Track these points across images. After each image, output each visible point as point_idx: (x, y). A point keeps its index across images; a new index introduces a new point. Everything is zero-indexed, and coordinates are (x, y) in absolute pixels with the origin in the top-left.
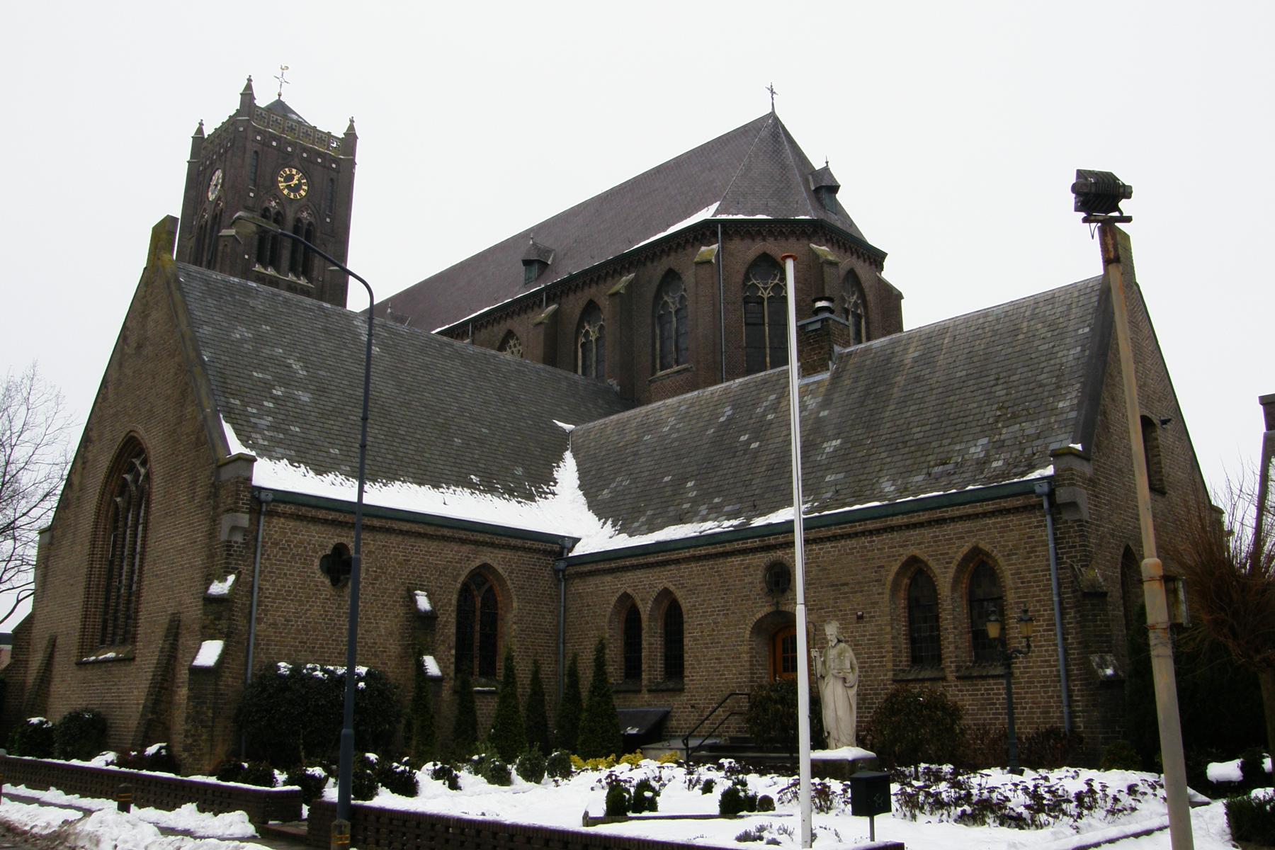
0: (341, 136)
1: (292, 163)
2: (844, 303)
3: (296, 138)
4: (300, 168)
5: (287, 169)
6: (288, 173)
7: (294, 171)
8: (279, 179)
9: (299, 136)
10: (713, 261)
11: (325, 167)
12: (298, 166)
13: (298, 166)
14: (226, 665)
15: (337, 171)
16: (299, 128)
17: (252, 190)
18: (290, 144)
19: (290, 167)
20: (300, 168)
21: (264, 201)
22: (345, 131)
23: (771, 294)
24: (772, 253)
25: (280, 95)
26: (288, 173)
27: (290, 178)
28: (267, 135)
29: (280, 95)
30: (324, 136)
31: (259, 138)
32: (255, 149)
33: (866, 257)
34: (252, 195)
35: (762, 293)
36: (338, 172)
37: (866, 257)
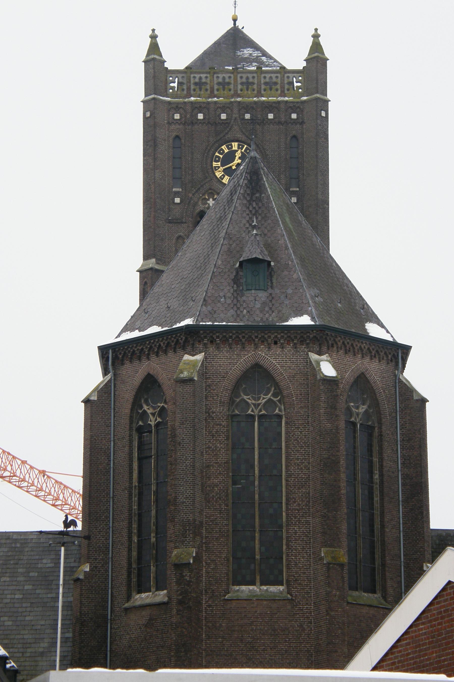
0: (300, 65)
1: (229, 136)
2: (351, 416)
3: (232, 96)
4: (244, 138)
5: (224, 147)
6: (226, 151)
7: (235, 146)
8: (215, 164)
9: (236, 91)
10: (196, 379)
11: (280, 123)
12: (239, 136)
13: (239, 136)
14: (168, 551)
15: (300, 122)
16: (235, 80)
17: (177, 194)
18: (223, 108)
19: (228, 142)
20: (244, 138)
21: (196, 204)
22: (305, 55)
23: (263, 412)
24: (265, 364)
25: (235, 20)
26: (226, 151)
27: (231, 156)
28: (189, 108)
29: (235, 20)
30: (273, 75)
31: (177, 116)
32: (174, 134)
33: (382, 354)
34: (177, 200)
35: (252, 411)
36: (302, 123)
37: (382, 354)
